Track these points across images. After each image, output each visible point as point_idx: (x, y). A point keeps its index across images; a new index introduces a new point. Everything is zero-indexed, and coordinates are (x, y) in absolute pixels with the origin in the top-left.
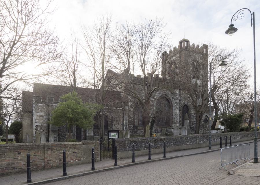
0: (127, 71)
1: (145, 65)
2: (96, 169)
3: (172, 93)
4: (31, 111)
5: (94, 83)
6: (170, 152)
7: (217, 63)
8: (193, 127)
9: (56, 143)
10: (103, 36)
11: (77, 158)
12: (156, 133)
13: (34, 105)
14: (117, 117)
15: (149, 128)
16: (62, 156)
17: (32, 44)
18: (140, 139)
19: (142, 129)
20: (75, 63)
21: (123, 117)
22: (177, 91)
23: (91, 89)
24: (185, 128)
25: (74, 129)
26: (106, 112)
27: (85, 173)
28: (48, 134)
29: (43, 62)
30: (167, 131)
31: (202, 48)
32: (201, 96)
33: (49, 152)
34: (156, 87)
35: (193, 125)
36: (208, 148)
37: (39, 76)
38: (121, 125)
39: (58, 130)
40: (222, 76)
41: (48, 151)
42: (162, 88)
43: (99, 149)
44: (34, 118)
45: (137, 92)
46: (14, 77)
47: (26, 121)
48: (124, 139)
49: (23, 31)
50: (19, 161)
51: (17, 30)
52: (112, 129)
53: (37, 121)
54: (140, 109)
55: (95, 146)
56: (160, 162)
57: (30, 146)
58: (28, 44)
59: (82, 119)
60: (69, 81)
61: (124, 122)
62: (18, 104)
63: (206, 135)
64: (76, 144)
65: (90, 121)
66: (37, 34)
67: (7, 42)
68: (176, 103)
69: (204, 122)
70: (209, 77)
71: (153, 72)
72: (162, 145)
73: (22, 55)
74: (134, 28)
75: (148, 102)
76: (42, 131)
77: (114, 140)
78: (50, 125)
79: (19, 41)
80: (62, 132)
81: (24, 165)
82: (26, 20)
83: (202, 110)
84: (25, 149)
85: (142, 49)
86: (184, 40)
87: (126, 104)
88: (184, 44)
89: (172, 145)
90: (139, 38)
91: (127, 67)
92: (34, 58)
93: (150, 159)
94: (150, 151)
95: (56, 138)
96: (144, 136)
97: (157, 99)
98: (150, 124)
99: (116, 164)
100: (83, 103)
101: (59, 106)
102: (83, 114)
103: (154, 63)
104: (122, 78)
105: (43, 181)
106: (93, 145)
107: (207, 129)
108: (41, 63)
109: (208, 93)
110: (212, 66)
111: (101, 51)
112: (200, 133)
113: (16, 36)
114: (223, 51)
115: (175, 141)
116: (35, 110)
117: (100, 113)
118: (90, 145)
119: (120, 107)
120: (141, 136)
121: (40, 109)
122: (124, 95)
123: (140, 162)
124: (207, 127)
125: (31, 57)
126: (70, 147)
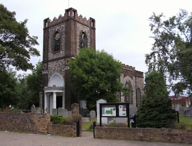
88: (71, 14)
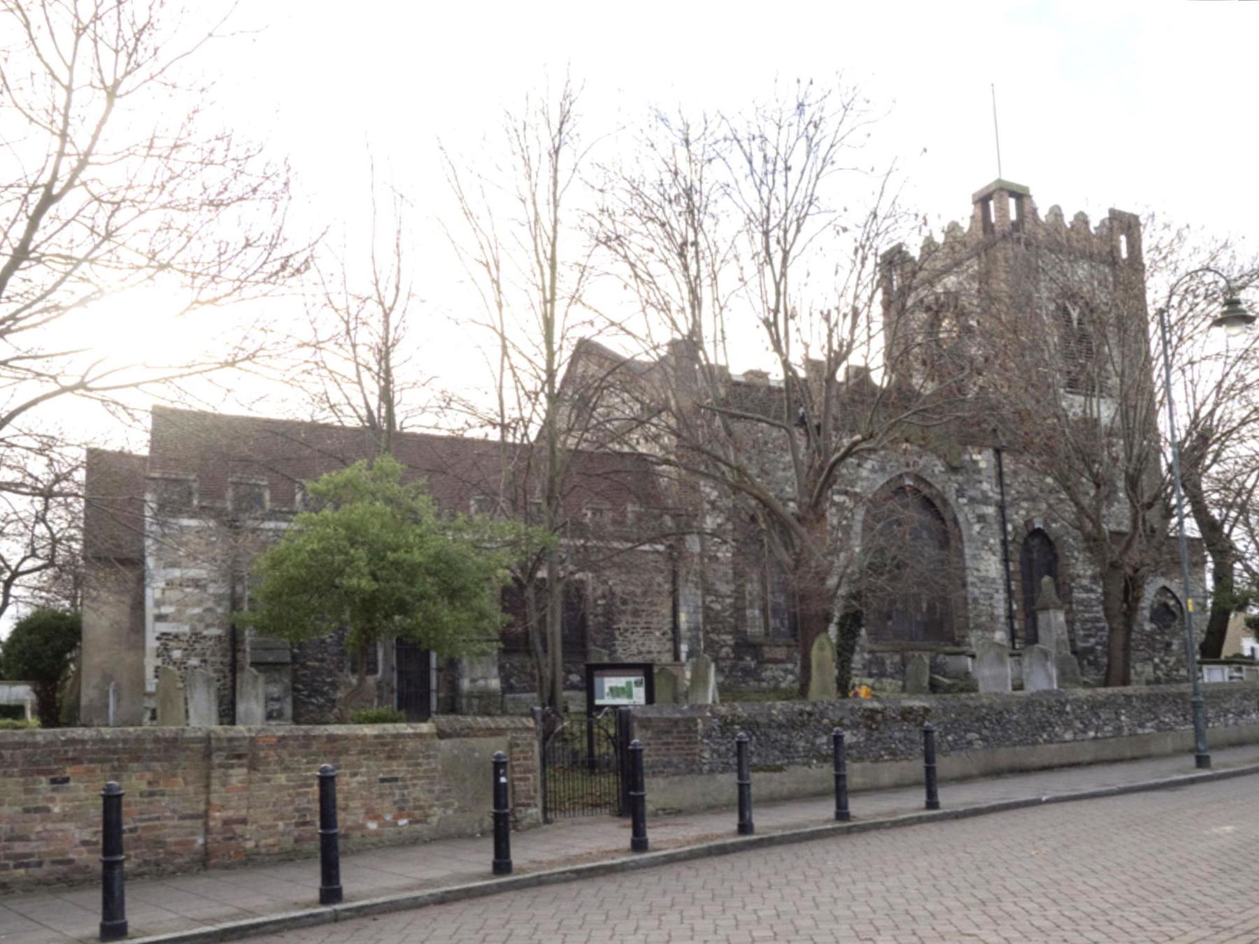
0: (688, 347)
1: (790, 316)
2: (522, 870)
3: (953, 469)
4: (135, 556)
5: (497, 409)
6: (964, 779)
7: (1198, 309)
8: (1091, 650)
9: (283, 729)
10: (546, 158)
11: (401, 809)
12: (870, 681)
13: (154, 528)
14: (639, 591)
15: (829, 654)
16: (317, 796)
17: (150, 198)
18: (778, 708)
19: (789, 659)
20: (388, 304)
21: (674, 593)
22: (984, 460)
23: (485, 442)
24: (1045, 654)
25: (384, 655)
26: (571, 568)
27: (456, 887)
28: (228, 680)
29: (208, 294)
30: (935, 668)
31: (1105, 231)
32: (1121, 484)
33: (238, 775)
34: (858, 437)
35: (1092, 640)
36: (1191, 760)
37: (186, 371)
38: (664, 634)
39: (288, 659)
40: (1232, 378)
41: (231, 772)
42: (894, 441)
43: (537, 762)
44: (152, 594)
45: (750, 459)
46: (39, 375)
47: (105, 609)
48: (686, 707)
49: (99, 128)
50: (54, 822)
51: (66, 123)
52: (610, 655)
53: (165, 610)
54: (770, 552)
55: (511, 746)
56: (909, 831)
57: (125, 741)
58: (123, 200)
59: (435, 604)
60: (358, 400)
61: (683, 617)
62: (59, 519)
63: (1174, 689)
64: (398, 736)
65: (480, 613)
66: (176, 146)
67: (11, 186)
68: (981, 518)
69: (1152, 620)
70: (1159, 383)
71: (837, 358)
72: (912, 742)
73: (91, 257)
74: (719, 118)
75: (814, 511)
76: (194, 662)
77: (622, 717)
78: (242, 633)
79: (77, 182)
80: (317, 672)
81: (85, 843)
82: (120, 73)
83: (1134, 556)
84: (91, 761)
85: (766, 233)
86: (1001, 189)
87: (686, 522)
88: (1003, 211)
89: (970, 743)
90: (748, 172)
91: (685, 327)
92: (161, 273)
93: (842, 814)
94: (844, 776)
95: (278, 700)
96: (803, 692)
97: (870, 496)
98: (833, 630)
99: (639, 844)
100: (438, 516)
101: (300, 532)
102: (435, 574)
103: (837, 309)
104: (657, 384)
105: (196, 931)
106: (500, 739)
107: (1172, 660)
108: (197, 302)
109: (1164, 468)
110: (1171, 327)
111: (535, 239)
112: (1138, 682)
113: (61, 154)
114: (1225, 246)
115: (991, 722)
116: (159, 549)
117: (535, 568)
118: (483, 739)
119: (652, 541)
120: (787, 695)
121: (186, 544)
122: (674, 476)
123: (788, 832)
124: (1174, 647)
125: (139, 268)
126: (362, 752)
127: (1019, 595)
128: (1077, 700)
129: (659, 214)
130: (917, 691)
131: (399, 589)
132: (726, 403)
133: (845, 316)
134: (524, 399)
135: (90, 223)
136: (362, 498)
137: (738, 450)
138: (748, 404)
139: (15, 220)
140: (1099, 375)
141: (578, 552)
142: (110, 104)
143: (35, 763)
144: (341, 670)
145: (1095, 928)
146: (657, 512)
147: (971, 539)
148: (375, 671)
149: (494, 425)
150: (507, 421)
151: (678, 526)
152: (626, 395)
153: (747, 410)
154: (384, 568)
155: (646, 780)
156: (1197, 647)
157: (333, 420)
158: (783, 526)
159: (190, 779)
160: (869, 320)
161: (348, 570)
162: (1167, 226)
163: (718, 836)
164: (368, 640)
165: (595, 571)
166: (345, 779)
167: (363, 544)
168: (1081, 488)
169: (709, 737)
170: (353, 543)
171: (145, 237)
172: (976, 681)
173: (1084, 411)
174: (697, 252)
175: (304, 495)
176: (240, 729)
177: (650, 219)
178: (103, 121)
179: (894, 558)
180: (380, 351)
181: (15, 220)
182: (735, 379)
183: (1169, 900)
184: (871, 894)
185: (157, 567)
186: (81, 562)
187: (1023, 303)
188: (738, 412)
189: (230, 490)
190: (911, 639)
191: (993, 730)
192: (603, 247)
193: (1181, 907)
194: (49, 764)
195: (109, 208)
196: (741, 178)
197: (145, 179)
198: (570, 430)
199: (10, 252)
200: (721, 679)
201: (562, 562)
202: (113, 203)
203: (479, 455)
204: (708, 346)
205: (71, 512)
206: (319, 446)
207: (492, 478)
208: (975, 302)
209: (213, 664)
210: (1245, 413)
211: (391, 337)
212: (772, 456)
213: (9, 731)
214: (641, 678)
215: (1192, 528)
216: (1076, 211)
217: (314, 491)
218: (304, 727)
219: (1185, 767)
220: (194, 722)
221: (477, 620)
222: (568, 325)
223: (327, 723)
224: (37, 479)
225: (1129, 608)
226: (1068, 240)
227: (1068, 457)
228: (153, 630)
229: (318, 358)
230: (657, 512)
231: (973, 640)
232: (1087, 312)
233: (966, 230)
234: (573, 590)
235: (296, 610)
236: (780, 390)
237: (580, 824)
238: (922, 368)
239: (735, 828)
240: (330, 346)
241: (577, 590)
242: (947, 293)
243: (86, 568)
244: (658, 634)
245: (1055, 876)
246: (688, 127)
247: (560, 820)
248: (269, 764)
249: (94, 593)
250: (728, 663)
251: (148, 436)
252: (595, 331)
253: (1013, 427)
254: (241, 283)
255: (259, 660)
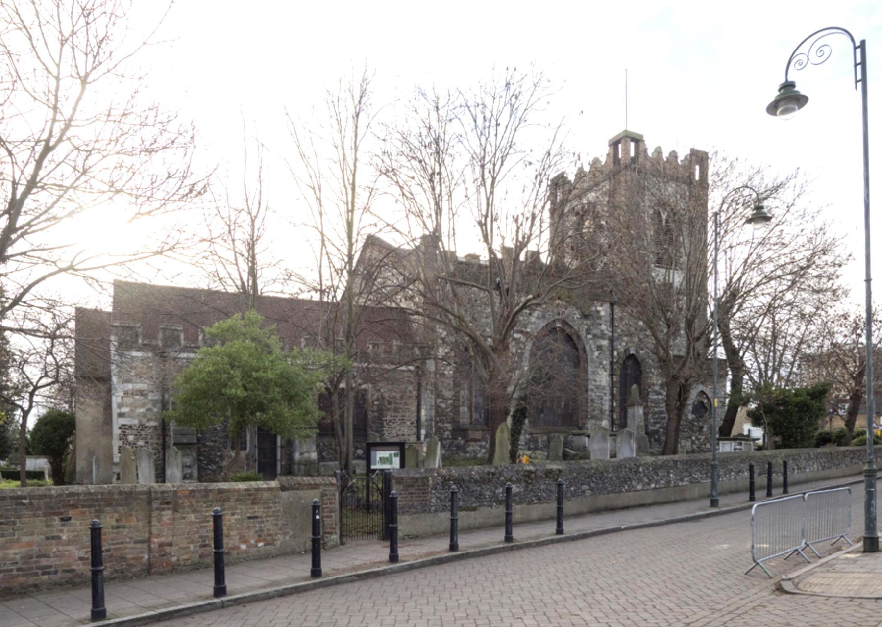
0: (433, 239)
2: (327, 575)
3: (585, 316)
5: (318, 280)
6: (579, 515)
7: (738, 212)
8: (657, 432)
9: (192, 485)
10: (351, 120)
11: (260, 536)
12: (529, 453)
13: (116, 358)
14: (398, 396)
16: (212, 528)
17: (109, 147)
19: (483, 439)
21: (419, 397)
24: (630, 435)
25: (250, 437)
26: (360, 381)
27: (290, 586)
28: (161, 454)
29: (146, 208)
30: (567, 444)
31: (687, 163)
32: (682, 325)
33: (167, 515)
34: (530, 296)
35: (658, 426)
36: (707, 502)
38: (412, 423)
39: (195, 441)
40: (754, 256)
41: (163, 513)
43: (337, 506)
44: (116, 400)
45: (466, 311)
46: (45, 261)
47: (89, 409)
48: (423, 470)
49: (77, 103)
51: (57, 100)
53: (124, 410)
54: (476, 370)
55: (323, 495)
56: (545, 549)
57: (102, 494)
58: (93, 149)
59: (280, 405)
60: (236, 276)
61: (423, 412)
63: (701, 456)
64: (258, 490)
66: (124, 114)
67: (24, 141)
68: (599, 348)
69: (693, 412)
70: (711, 260)
72: (551, 491)
75: (502, 344)
77: (386, 476)
79: (64, 138)
80: (212, 449)
81: (81, 559)
82: (89, 68)
83: (686, 371)
84: (83, 506)
85: (483, 166)
86: (627, 136)
87: (427, 351)
88: (626, 151)
89: (583, 492)
91: (431, 227)
92: (117, 195)
93: (509, 538)
95: (189, 467)
96: (490, 460)
98: (509, 420)
100: (282, 349)
101: (202, 359)
102: (280, 386)
103: (523, 214)
104: (413, 264)
105: (145, 614)
106: (316, 491)
107: (703, 438)
108: (139, 213)
109: (709, 314)
110: (721, 224)
111: (343, 171)
112: (682, 452)
113: (54, 120)
114: (758, 172)
116: (119, 371)
117: (339, 382)
119: (407, 364)
120: (481, 462)
121: (135, 368)
122: (421, 322)
123: (477, 550)
124: (705, 430)
125: (103, 192)
126: (237, 500)
127: (618, 397)
128: (646, 464)
129: (419, 155)
130: (555, 459)
131: (259, 395)
132: (454, 275)
133: (527, 218)
134: (334, 274)
135: (73, 164)
136: (238, 338)
137: (459, 305)
138: (466, 275)
139: (28, 162)
140: (676, 255)
141: (364, 371)
142: (83, 88)
143: (51, 508)
144: (226, 448)
145: (646, 610)
146: (410, 345)
147: (593, 361)
148: (245, 448)
149: (316, 291)
150: (324, 288)
151: (422, 354)
152: (395, 271)
153: (466, 279)
154: (250, 382)
155: (399, 517)
156: (717, 429)
157: (221, 288)
158: (484, 354)
159: (139, 518)
160: (542, 221)
161: (230, 383)
162: (724, 159)
163: (438, 553)
164: (241, 428)
165: (373, 383)
166: (228, 517)
167: (238, 367)
168: (659, 328)
169: (435, 489)
170: (232, 367)
171: (108, 172)
172: (589, 452)
173: (665, 279)
174: (440, 179)
175: (204, 336)
176: (168, 486)
177: (413, 158)
178: (79, 99)
179: (547, 374)
180: (249, 244)
181: (28, 162)
182: (460, 260)
183: (688, 592)
184: (522, 589)
185: (118, 382)
186: (74, 380)
187: (634, 209)
188: (460, 281)
189: (160, 333)
190: (554, 425)
191: (597, 484)
192: (384, 176)
193: (694, 597)
194: (59, 508)
195: (84, 154)
196: (469, 131)
197: (106, 135)
198: (361, 293)
199: (25, 183)
200: (444, 452)
201: (354, 378)
202: (87, 151)
203: (307, 309)
204: (445, 239)
205: (68, 348)
206: (212, 305)
207: (315, 324)
208: (605, 209)
209: (152, 444)
210: (759, 279)
211: (255, 235)
212: (479, 309)
213: (36, 488)
214: (398, 452)
215: (721, 353)
216: (671, 150)
217: (210, 333)
218: (204, 484)
219: (703, 507)
220: (142, 481)
221: (304, 415)
222: (361, 226)
223: (218, 481)
224: (46, 327)
225: (681, 405)
226: (664, 169)
227: (653, 308)
228: (117, 422)
229: (212, 249)
230: (410, 345)
231: (589, 426)
232: (672, 215)
233: (603, 163)
234: (360, 395)
235: (200, 409)
236: (486, 267)
237: (361, 545)
238: (571, 252)
239: (448, 547)
240: (219, 241)
241: (363, 395)
242: (589, 203)
243: (77, 383)
244: (408, 423)
245: (626, 577)
246: (438, 98)
247: (350, 543)
248: (184, 507)
249: (82, 400)
250: (448, 442)
251: (111, 299)
252: (377, 230)
253: (622, 289)
254: (165, 201)
255: (178, 441)
